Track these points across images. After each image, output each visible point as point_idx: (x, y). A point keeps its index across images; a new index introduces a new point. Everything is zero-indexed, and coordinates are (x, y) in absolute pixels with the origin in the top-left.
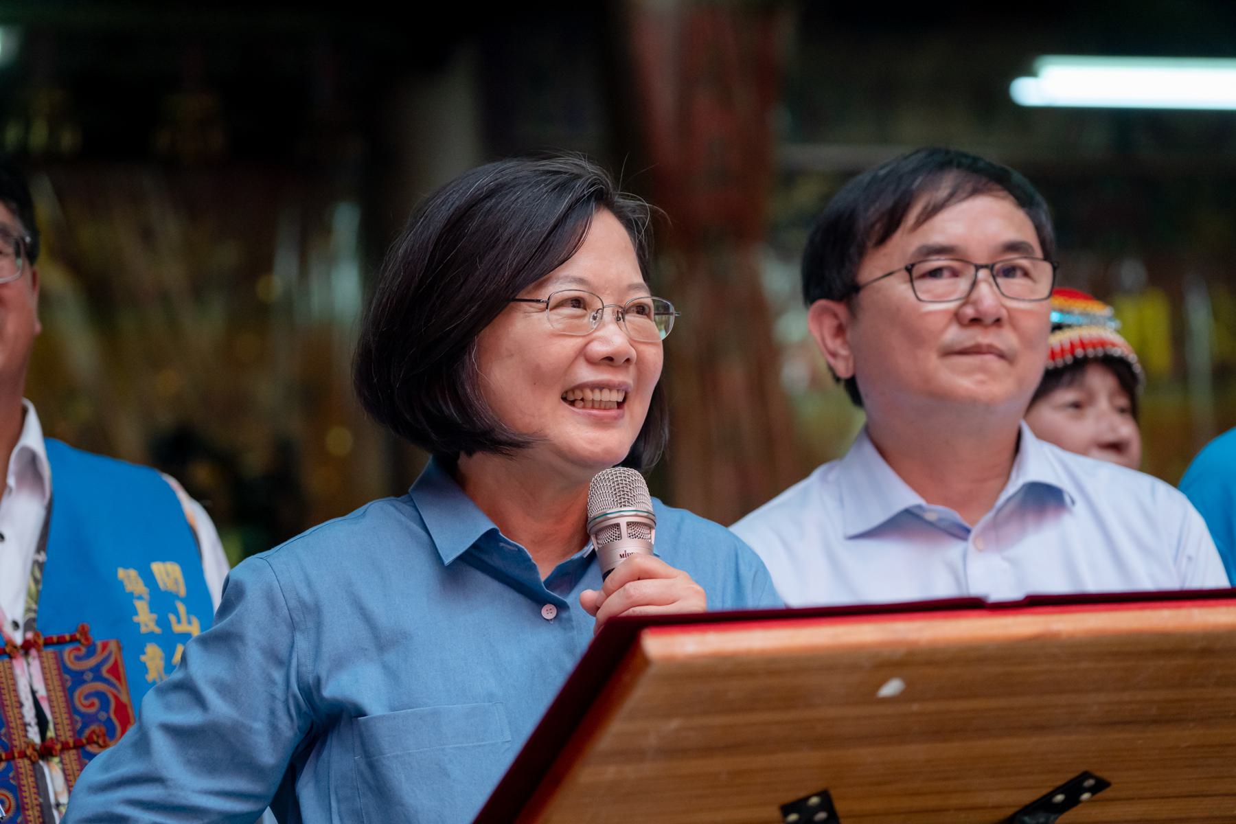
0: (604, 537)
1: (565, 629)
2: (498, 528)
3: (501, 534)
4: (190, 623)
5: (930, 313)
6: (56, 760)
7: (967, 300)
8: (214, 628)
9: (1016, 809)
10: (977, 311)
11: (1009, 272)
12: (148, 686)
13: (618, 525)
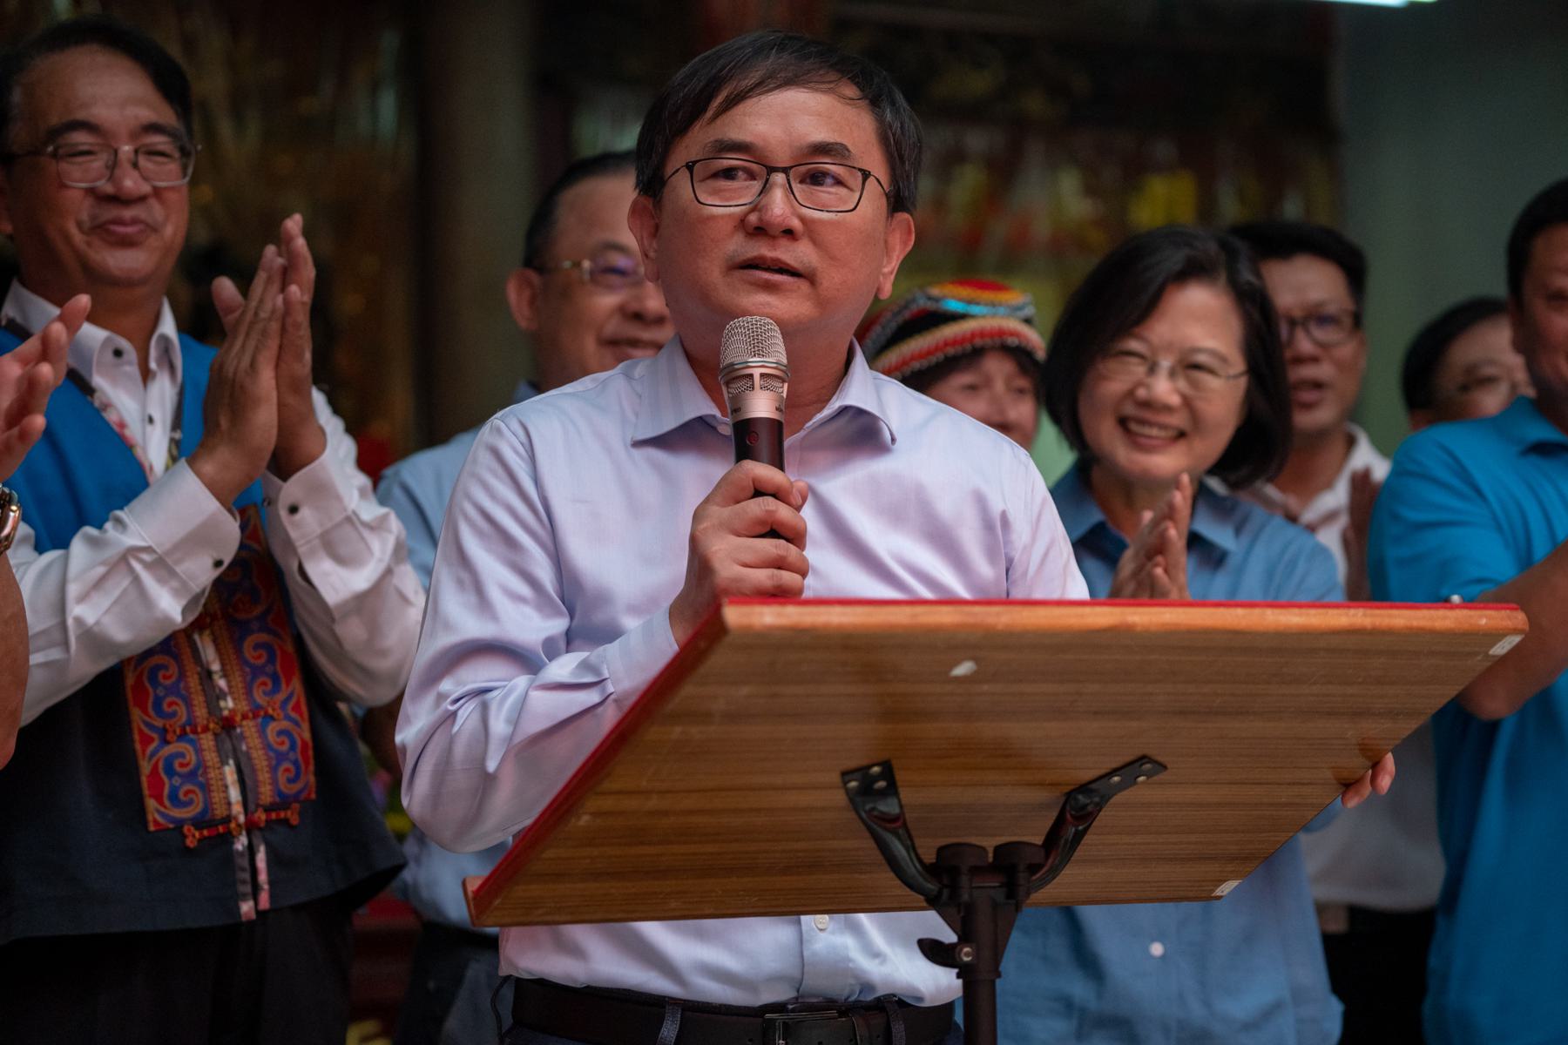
0: (737, 387)
5: (713, 218)
6: (207, 632)
7: (755, 208)
8: (814, 420)
9: (1072, 787)
10: (760, 219)
11: (816, 178)
13: (751, 376)
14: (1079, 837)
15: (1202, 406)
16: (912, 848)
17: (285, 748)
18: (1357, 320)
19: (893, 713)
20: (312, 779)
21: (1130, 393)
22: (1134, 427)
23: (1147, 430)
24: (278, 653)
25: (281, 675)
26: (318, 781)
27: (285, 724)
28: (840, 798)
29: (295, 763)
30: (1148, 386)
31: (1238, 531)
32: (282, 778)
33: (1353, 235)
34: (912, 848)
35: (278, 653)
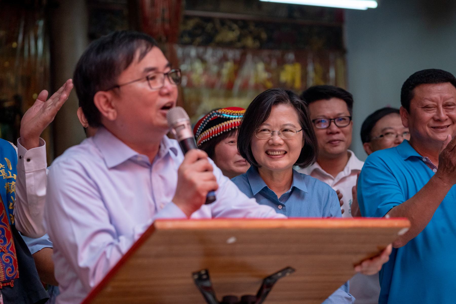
1: (284, 211)
2: (267, 186)
3: (268, 187)
4: (13, 175)
12: (275, 80)
14: (267, 293)
15: (290, 142)
16: (214, 297)
17: (8, 262)
18: (350, 118)
19: (209, 254)
20: (18, 271)
21: (268, 142)
22: (270, 153)
23: (275, 153)
24: (5, 231)
25: (6, 238)
26: (19, 272)
27: (8, 254)
28: (191, 281)
29: (12, 267)
30: (272, 139)
31: (307, 185)
32: (7, 272)
33: (350, 91)
34: (214, 297)
35: (5, 231)
